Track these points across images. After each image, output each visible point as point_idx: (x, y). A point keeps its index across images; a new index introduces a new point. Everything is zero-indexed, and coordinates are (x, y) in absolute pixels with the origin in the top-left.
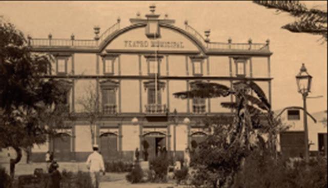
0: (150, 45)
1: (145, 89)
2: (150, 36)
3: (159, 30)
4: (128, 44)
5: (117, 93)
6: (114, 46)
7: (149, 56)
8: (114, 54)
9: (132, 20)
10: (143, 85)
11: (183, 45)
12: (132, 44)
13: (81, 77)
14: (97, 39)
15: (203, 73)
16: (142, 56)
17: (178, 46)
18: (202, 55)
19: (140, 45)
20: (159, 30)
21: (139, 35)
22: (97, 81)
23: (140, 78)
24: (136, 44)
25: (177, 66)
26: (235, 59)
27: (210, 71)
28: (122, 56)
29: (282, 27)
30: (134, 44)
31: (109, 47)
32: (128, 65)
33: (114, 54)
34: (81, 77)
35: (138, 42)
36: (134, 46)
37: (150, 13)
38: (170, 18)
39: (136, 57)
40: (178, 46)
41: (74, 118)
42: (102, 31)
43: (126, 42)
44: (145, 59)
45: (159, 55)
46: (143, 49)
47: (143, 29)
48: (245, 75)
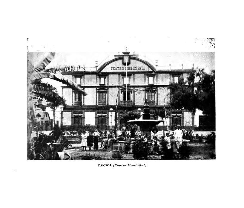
0: (124, 68)
1: (121, 93)
2: (124, 64)
3: (129, 61)
4: (113, 69)
5: (107, 95)
6: (107, 69)
7: (123, 74)
8: (106, 75)
9: (115, 56)
10: (120, 90)
11: (143, 68)
12: (115, 69)
13: (112, 87)
14: (97, 67)
15: (105, 84)
16: (120, 75)
17: (140, 69)
18: (153, 73)
19: (119, 69)
20: (129, 61)
21: (119, 63)
22: (96, 88)
23: (118, 87)
24: (117, 69)
25: (166, 81)
26: (173, 75)
27: (109, 83)
28: (110, 76)
29: (54, 57)
30: (116, 69)
31: (103, 71)
32: (113, 80)
33: (106, 75)
34: (112, 87)
35: (118, 68)
36: (116, 69)
37: (125, 51)
38: (136, 53)
39: (117, 76)
40: (140, 69)
41: (116, 109)
42: (99, 63)
43: (111, 68)
44: (122, 77)
45: (130, 74)
46: (119, 71)
47: (121, 60)
48: (105, 85)
